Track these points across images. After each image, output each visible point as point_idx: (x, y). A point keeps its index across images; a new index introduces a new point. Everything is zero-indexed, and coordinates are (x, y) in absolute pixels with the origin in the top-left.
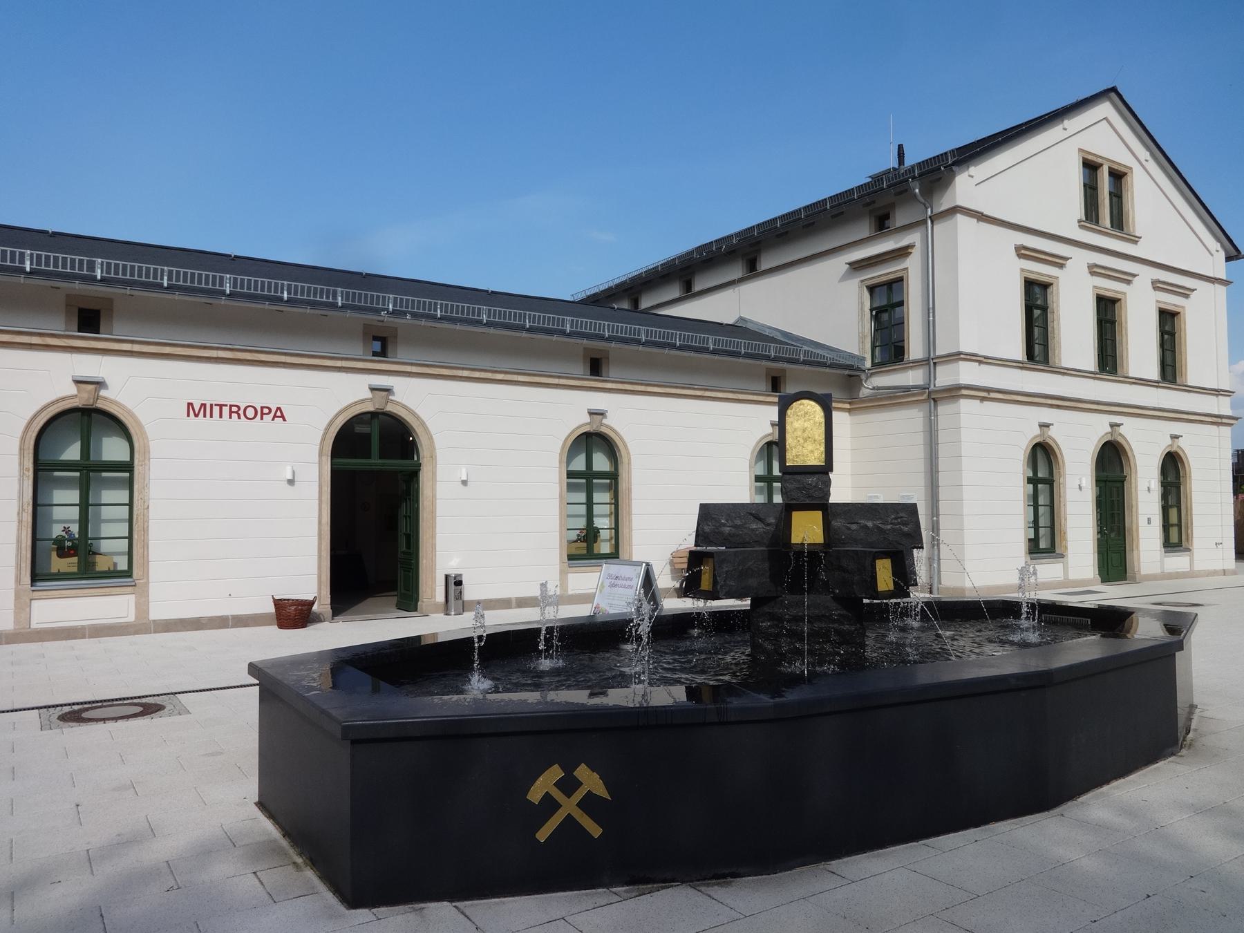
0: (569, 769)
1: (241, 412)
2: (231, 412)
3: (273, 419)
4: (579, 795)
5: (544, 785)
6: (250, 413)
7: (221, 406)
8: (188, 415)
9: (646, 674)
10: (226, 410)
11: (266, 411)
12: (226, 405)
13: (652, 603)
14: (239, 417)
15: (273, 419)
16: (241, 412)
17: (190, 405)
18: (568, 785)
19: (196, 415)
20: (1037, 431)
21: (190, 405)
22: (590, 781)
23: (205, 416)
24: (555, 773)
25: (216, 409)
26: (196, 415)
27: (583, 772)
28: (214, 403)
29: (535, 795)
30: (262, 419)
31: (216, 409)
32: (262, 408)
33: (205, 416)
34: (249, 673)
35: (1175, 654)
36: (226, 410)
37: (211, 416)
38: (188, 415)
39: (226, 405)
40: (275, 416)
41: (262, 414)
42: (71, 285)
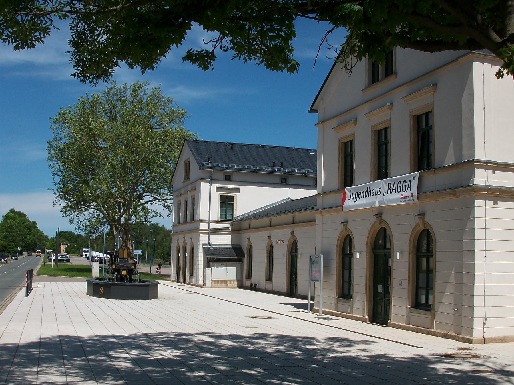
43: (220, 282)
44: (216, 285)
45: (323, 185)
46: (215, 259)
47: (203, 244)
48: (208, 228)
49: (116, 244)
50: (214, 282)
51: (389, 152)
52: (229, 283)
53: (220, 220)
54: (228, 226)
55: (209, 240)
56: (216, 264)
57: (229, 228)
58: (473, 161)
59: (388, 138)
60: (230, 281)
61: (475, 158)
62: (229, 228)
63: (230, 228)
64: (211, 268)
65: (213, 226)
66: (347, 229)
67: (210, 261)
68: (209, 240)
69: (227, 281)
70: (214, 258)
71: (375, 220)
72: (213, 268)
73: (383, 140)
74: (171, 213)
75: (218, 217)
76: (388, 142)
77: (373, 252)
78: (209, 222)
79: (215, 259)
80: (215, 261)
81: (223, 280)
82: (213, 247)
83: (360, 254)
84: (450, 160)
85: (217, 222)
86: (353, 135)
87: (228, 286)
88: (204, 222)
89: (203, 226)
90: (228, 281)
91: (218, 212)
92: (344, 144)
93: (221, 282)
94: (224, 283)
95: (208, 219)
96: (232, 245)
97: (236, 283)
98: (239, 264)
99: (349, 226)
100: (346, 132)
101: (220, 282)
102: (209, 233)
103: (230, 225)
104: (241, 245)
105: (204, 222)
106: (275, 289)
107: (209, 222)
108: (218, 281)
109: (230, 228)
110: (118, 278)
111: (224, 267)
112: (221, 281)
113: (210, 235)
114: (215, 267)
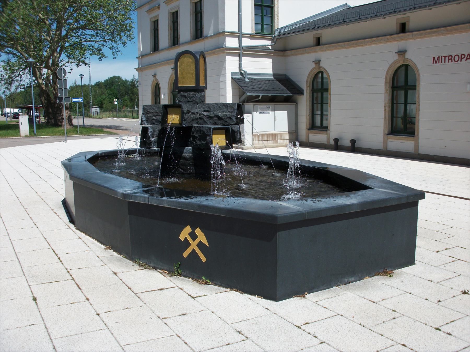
0: (194, 228)
1: (453, 59)
2: (449, 59)
3: (466, 61)
4: (197, 241)
5: (185, 233)
6: (456, 58)
7: (445, 57)
8: (433, 63)
9: (217, 194)
10: (447, 58)
11: (463, 56)
12: (447, 56)
13: (300, 167)
14: (452, 62)
15: (466, 61)
16: (453, 59)
17: (434, 58)
18: (193, 236)
19: (436, 63)
20: (313, 65)
21: (434, 58)
22: (201, 237)
23: (439, 63)
24: (188, 229)
25: (443, 58)
26: (436, 63)
27: (198, 231)
28: (442, 56)
29: (182, 237)
30: (461, 61)
31: (443, 58)
32: (462, 55)
33: (439, 63)
34: (70, 179)
35: (418, 202)
36: (447, 58)
37: (441, 63)
38: (433, 63)
39: (447, 56)
40: (467, 59)
41: (462, 58)
42: (78, 100)
43: (265, 138)
44: (261, 142)
45: (141, 50)
46: (260, 98)
47: (233, 74)
48: (238, 47)
49: (59, 86)
50: (257, 138)
51: (203, 19)
52: (279, 138)
53: (256, 33)
54: (267, 43)
55: (240, 65)
56: (259, 106)
57: (269, 47)
58: (224, 32)
59: (202, 8)
60: (281, 134)
61: (226, 30)
62: (269, 47)
63: (270, 47)
64: (251, 113)
65: (246, 42)
66: (156, 80)
67: (244, 103)
68: (240, 65)
69: (275, 135)
70: (259, 96)
71: (172, 72)
72: (254, 113)
73: (199, 10)
74: (10, 85)
75: (252, 28)
76: (202, 11)
77: (172, 94)
78: (239, 35)
79: (260, 98)
80: (259, 101)
81: (270, 134)
82: (248, 79)
83: (164, 95)
84: (211, 33)
85: (251, 37)
86: (158, 16)
87: (277, 143)
88: (232, 34)
89: (231, 42)
90: (277, 134)
91: (252, 20)
92: (172, 14)
93: (268, 137)
94: (272, 139)
95: (237, 30)
96: (274, 75)
97: (287, 137)
98: (291, 106)
99: (157, 77)
100: (154, 14)
101: (265, 138)
102: (241, 54)
103: (270, 42)
104: (287, 75)
105: (232, 34)
106: (422, 150)
107: (239, 35)
108: (263, 135)
109: (270, 47)
110: (185, 159)
111: (272, 111)
112: (268, 135)
113: (242, 57)
114: (258, 112)
